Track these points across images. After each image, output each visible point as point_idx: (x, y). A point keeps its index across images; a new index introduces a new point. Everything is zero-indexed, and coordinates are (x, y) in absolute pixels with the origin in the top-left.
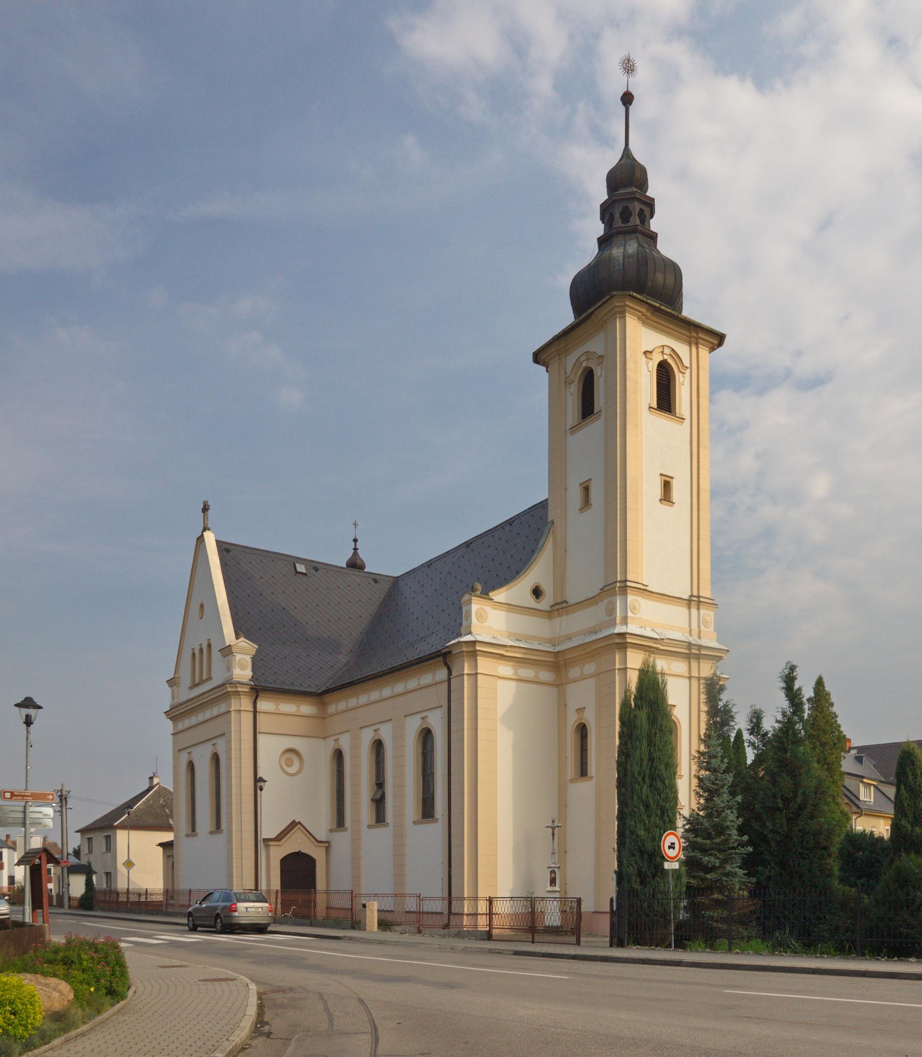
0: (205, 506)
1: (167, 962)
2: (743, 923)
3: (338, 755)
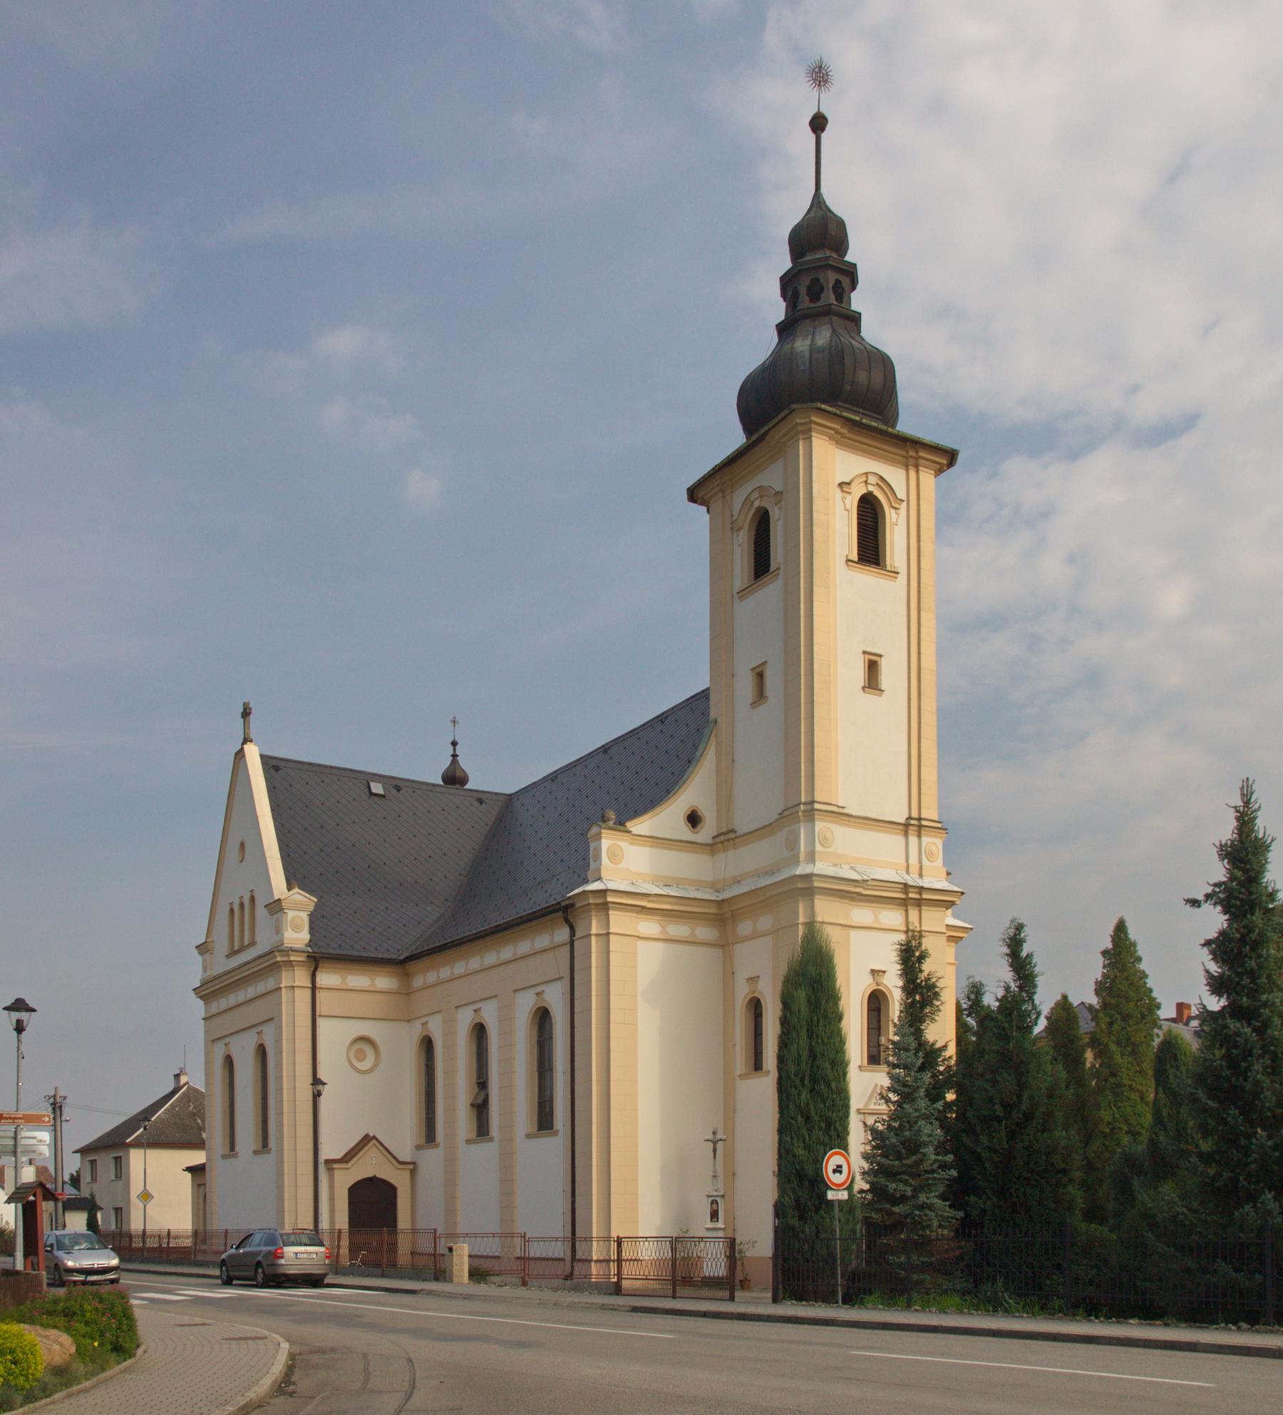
0: (245, 709)
1: (187, 1320)
2: (948, 1273)
3: (427, 1045)
